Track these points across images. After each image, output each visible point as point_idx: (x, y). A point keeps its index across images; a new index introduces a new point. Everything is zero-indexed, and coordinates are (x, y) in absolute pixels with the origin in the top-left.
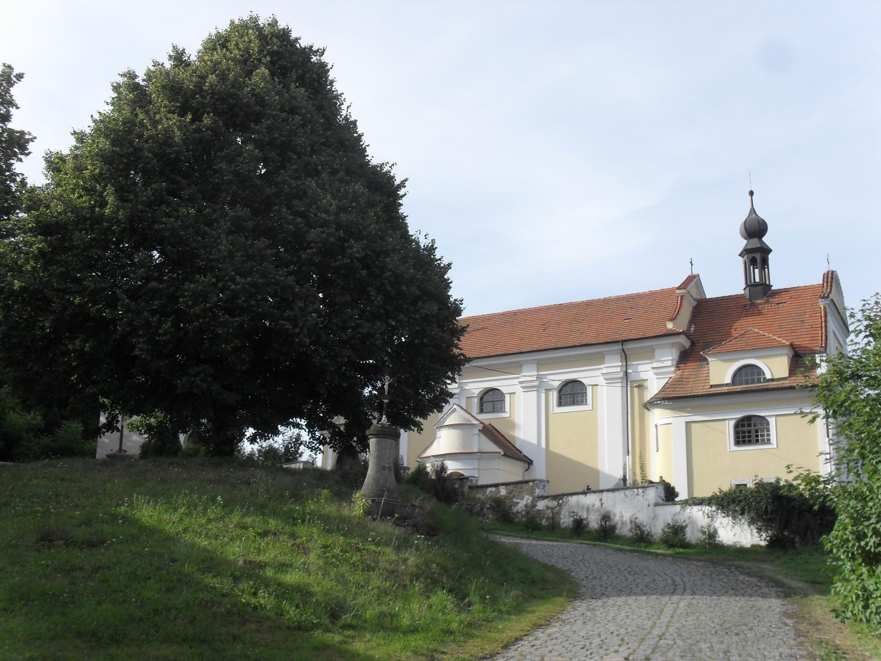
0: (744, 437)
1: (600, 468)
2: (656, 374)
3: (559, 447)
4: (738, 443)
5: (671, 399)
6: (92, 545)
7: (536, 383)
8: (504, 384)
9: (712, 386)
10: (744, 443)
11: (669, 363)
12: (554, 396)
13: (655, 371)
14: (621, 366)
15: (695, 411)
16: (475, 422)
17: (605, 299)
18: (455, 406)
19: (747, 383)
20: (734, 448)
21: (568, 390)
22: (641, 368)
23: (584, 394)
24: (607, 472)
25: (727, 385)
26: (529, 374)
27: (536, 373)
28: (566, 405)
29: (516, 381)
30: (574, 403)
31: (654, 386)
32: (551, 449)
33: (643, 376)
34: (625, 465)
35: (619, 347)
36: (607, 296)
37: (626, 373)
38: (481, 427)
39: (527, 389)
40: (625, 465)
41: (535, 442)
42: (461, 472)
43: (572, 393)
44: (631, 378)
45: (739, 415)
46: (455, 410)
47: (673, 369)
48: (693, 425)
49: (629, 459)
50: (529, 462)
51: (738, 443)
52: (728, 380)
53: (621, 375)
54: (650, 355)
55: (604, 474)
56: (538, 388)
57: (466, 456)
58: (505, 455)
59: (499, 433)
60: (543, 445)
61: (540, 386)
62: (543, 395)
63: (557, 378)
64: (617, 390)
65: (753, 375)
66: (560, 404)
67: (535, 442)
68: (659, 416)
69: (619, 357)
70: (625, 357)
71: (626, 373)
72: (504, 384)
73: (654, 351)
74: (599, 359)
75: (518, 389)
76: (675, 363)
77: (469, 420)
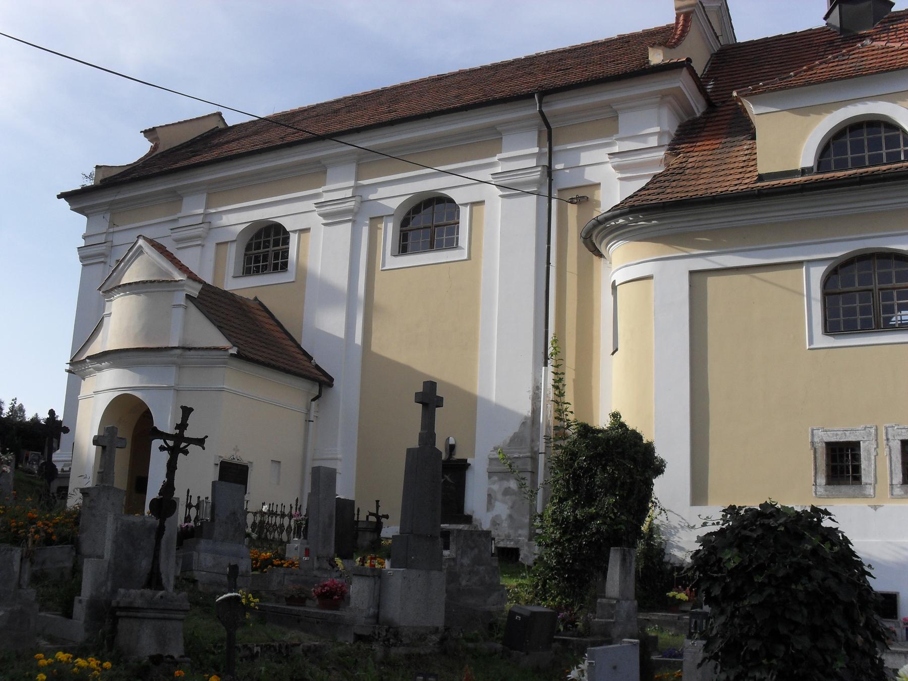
0: (850, 312)
1: (479, 392)
2: (617, 168)
3: (390, 345)
4: (830, 328)
5: (656, 212)
6: (291, 508)
7: (350, 205)
8: (291, 211)
9: (761, 178)
10: (850, 329)
11: (653, 142)
12: (388, 232)
13: (617, 160)
14: (539, 156)
15: (719, 241)
16: (178, 276)
17: (527, 59)
18: (141, 242)
19: (858, 163)
20: (831, 342)
21: (421, 220)
22: (586, 158)
23: (454, 226)
24: (494, 398)
25: (804, 171)
26: (338, 188)
27: (352, 183)
28: (417, 251)
29: (310, 205)
30: (432, 246)
31: (613, 190)
32: (375, 348)
33: (591, 176)
34: (537, 388)
35: (530, 110)
36: (532, 52)
37: (549, 171)
38: (195, 290)
39: (333, 218)
40: (537, 388)
41: (341, 334)
42: (138, 394)
43: (428, 223)
44: (562, 181)
45: (839, 251)
46: (140, 251)
47: (661, 154)
48: (711, 281)
49: (548, 376)
50: (323, 381)
51: (830, 328)
52: (807, 157)
53: (536, 175)
54: (605, 124)
55: (488, 402)
56: (353, 216)
57: (152, 357)
58: (238, 356)
59: (272, 316)
60: (358, 340)
61: (359, 213)
62: (365, 231)
63: (395, 191)
64: (529, 205)
65: (875, 144)
66: (403, 248)
67: (341, 334)
68: (623, 260)
69: (535, 135)
70: (549, 134)
71: (549, 171)
72: (291, 211)
73: (616, 118)
74: (488, 142)
75: (315, 220)
76: (667, 141)
77: (161, 271)
